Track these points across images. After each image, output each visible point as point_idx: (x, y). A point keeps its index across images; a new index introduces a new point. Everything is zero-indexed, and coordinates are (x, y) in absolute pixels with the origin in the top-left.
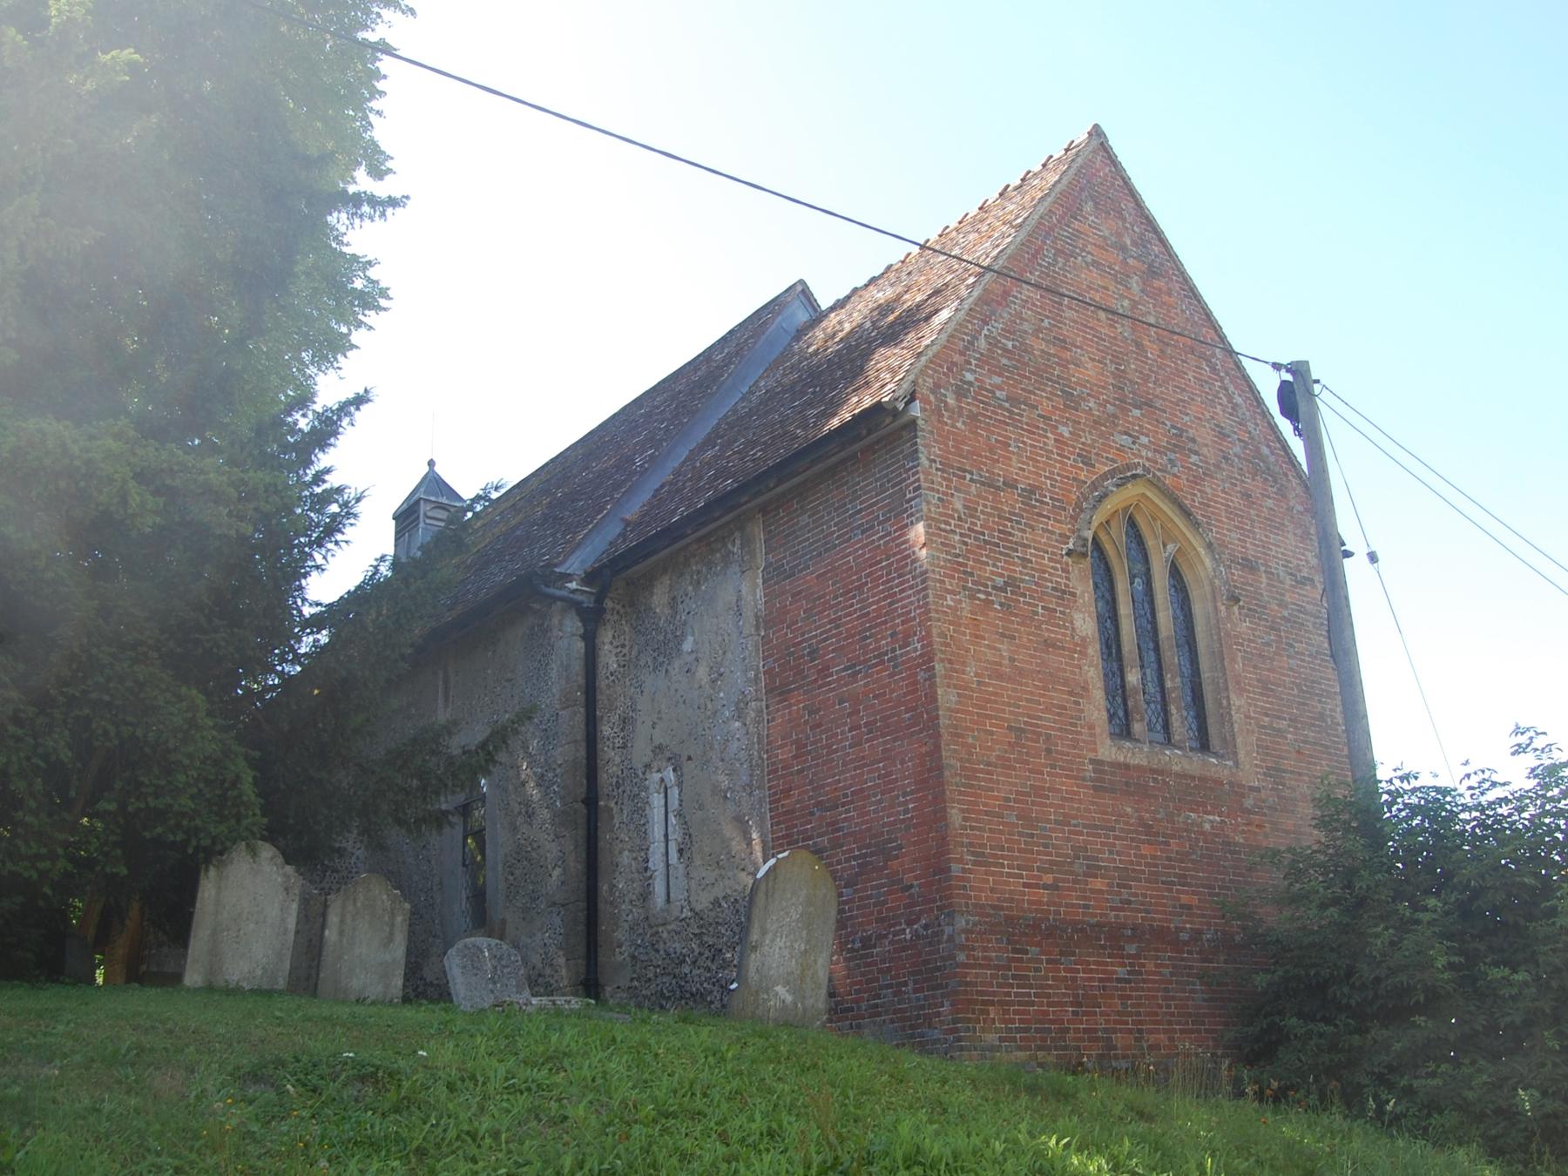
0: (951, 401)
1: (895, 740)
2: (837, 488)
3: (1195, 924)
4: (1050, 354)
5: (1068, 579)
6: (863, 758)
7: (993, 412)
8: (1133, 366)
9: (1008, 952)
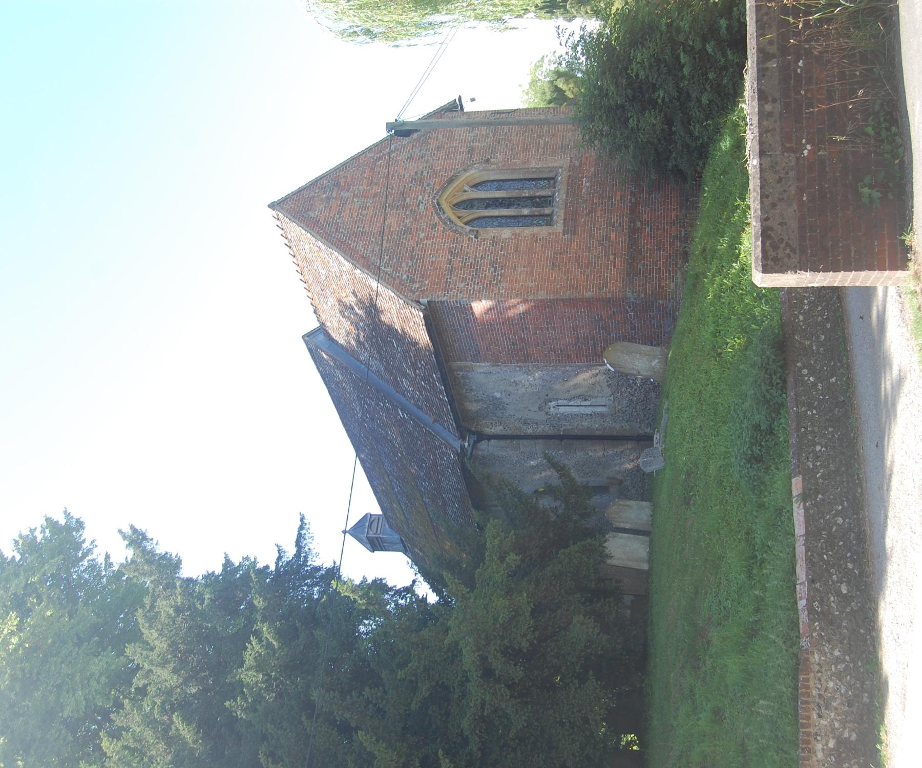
1: (556, 315)
5: (488, 239)
6: (560, 327)
7: (419, 267)
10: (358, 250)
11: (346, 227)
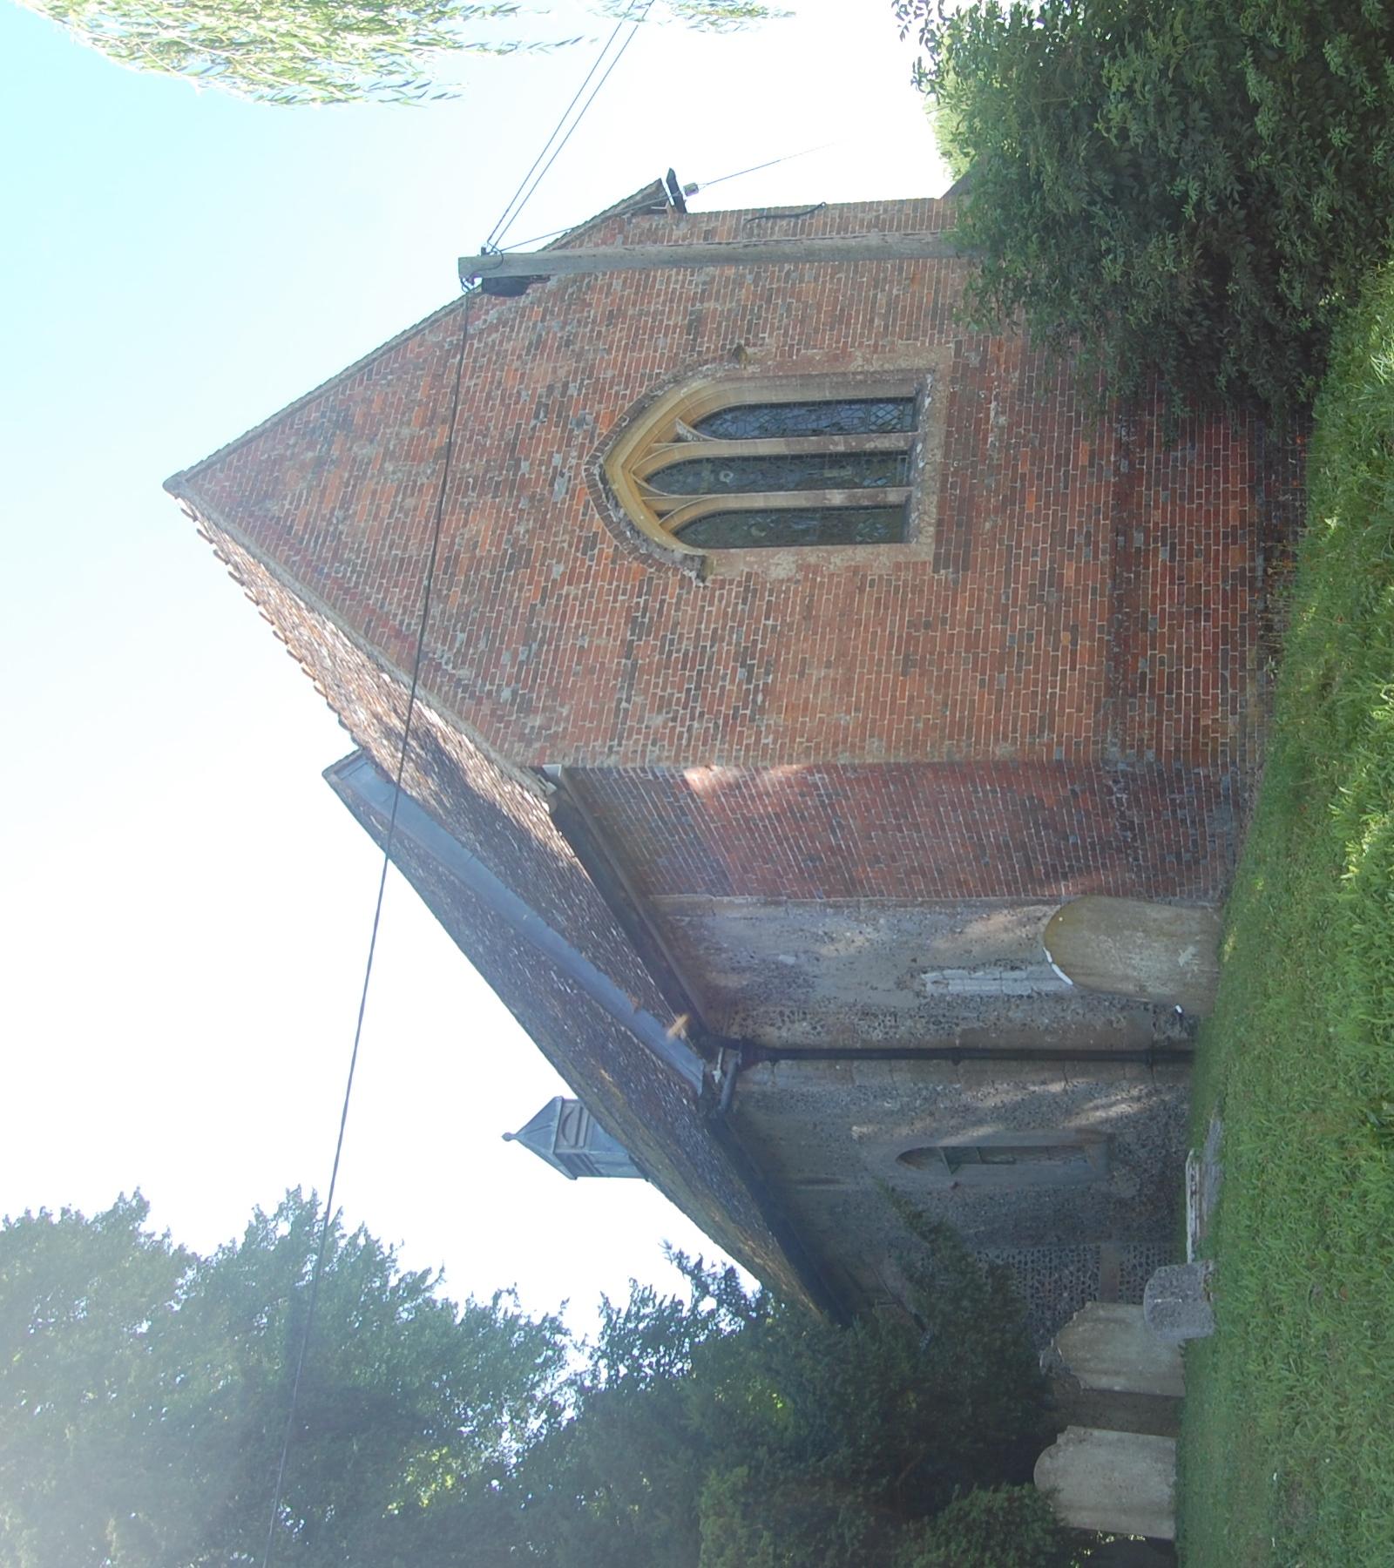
0: (538, 721)
1: (916, 798)
4: (467, 582)
5: (731, 583)
6: (933, 823)
8: (468, 466)
10: (387, 614)
11: (360, 544)
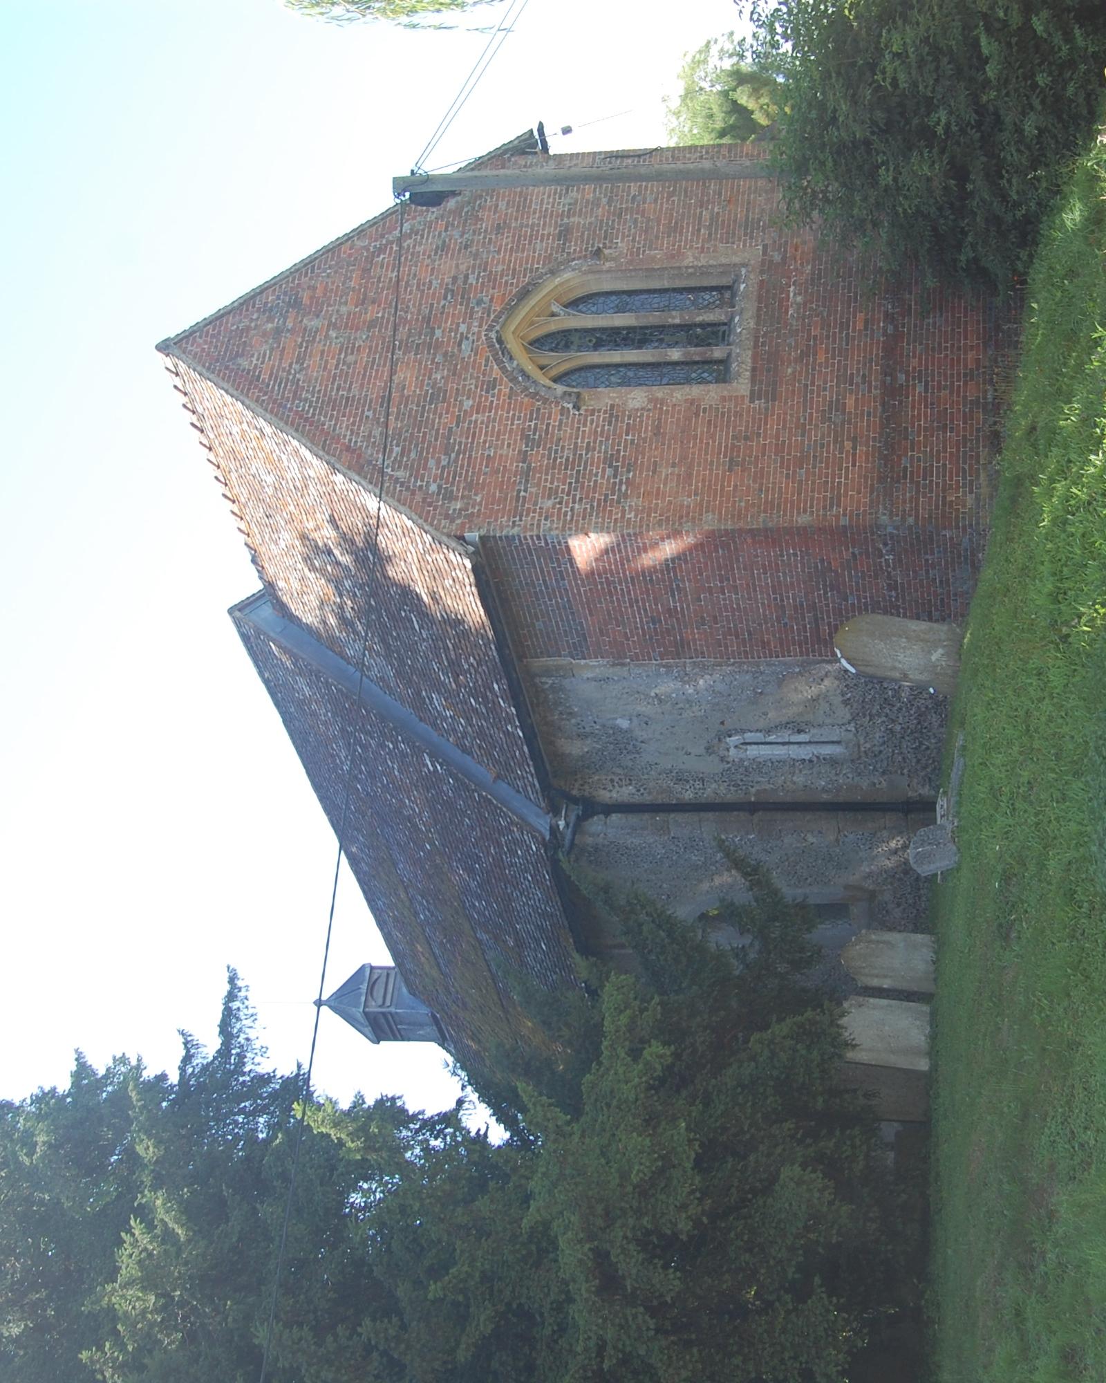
2: (519, 597)
3: (879, 318)
5: (599, 411)
6: (748, 585)
9: (905, 483)
